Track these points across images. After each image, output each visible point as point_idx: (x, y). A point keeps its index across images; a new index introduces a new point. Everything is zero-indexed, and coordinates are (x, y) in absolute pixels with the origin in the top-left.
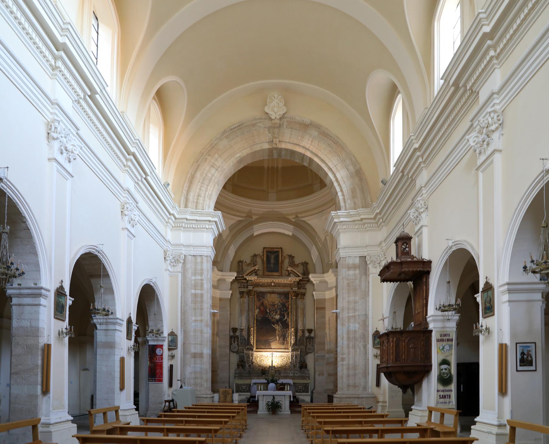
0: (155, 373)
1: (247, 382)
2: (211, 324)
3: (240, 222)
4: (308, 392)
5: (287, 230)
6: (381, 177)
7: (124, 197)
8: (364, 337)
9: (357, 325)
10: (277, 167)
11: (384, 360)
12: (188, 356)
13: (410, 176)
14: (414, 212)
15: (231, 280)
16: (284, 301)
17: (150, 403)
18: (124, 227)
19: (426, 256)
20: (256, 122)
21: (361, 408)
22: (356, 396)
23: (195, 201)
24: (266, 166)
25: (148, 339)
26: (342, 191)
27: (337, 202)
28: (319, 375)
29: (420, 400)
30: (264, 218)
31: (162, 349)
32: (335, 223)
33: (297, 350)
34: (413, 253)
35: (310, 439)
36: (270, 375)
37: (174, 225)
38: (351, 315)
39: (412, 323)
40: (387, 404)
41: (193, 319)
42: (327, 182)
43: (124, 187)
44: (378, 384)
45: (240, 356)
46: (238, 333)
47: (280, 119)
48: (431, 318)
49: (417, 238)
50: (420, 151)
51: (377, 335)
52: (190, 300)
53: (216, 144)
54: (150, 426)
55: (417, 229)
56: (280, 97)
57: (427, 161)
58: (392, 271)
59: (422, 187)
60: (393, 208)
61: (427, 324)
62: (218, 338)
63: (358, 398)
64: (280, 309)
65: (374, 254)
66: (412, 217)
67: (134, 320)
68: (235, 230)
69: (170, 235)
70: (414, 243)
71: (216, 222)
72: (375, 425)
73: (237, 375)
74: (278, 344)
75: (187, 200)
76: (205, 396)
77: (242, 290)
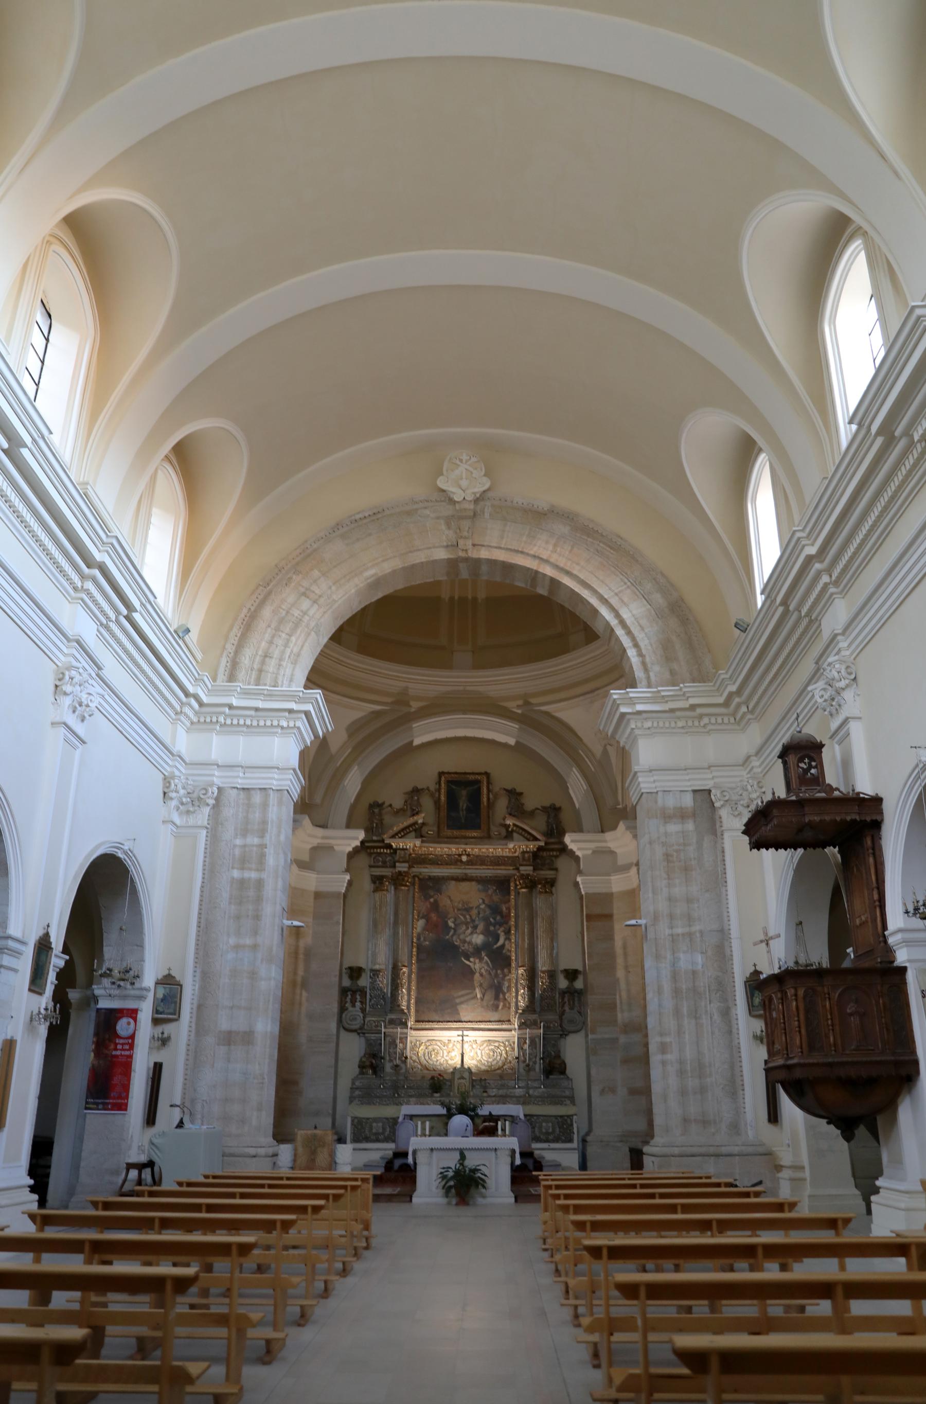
0: (107, 1087)
1: (388, 1111)
2: (281, 955)
3: (376, 714)
4: (570, 1140)
5: (504, 733)
6: (736, 614)
7: (65, 655)
8: (722, 987)
9: (699, 959)
10: (475, 599)
11: (777, 1046)
12: (210, 1040)
13: (804, 611)
14: (824, 689)
15: (350, 849)
16: (496, 898)
17: (82, 1171)
18: (58, 719)
19: (865, 786)
20: (415, 506)
21: (718, 1185)
22: (712, 1150)
23: (255, 666)
24: (445, 595)
25: (97, 992)
26: (636, 645)
27: (627, 670)
28: (602, 1092)
29: (898, 1161)
30: (436, 707)
31: (135, 1020)
32: (623, 715)
33: (533, 1024)
34: (832, 777)
35: (563, 1279)
36: (455, 1094)
37: (195, 720)
38: (679, 931)
39: (850, 950)
40: (807, 1174)
41: (232, 941)
42: (598, 627)
43: (70, 633)
44: (774, 1116)
45: (367, 1040)
46: (364, 981)
47: (476, 501)
48: (899, 936)
49: (837, 747)
50: (822, 562)
51: (757, 984)
52: (226, 895)
53: (315, 550)
54: (52, 1233)
55: (834, 725)
56: (474, 459)
57: (844, 581)
58: (775, 821)
59: (836, 635)
60: (771, 682)
61: (889, 951)
62: (304, 994)
63: (717, 1155)
64: (486, 919)
65: (733, 785)
66: (820, 700)
67: (57, 941)
68: (363, 735)
69: (183, 741)
70: (830, 757)
71: (307, 714)
72: (758, 1233)
73: (357, 1093)
75: (234, 665)
76: (252, 1151)
77: (378, 872)
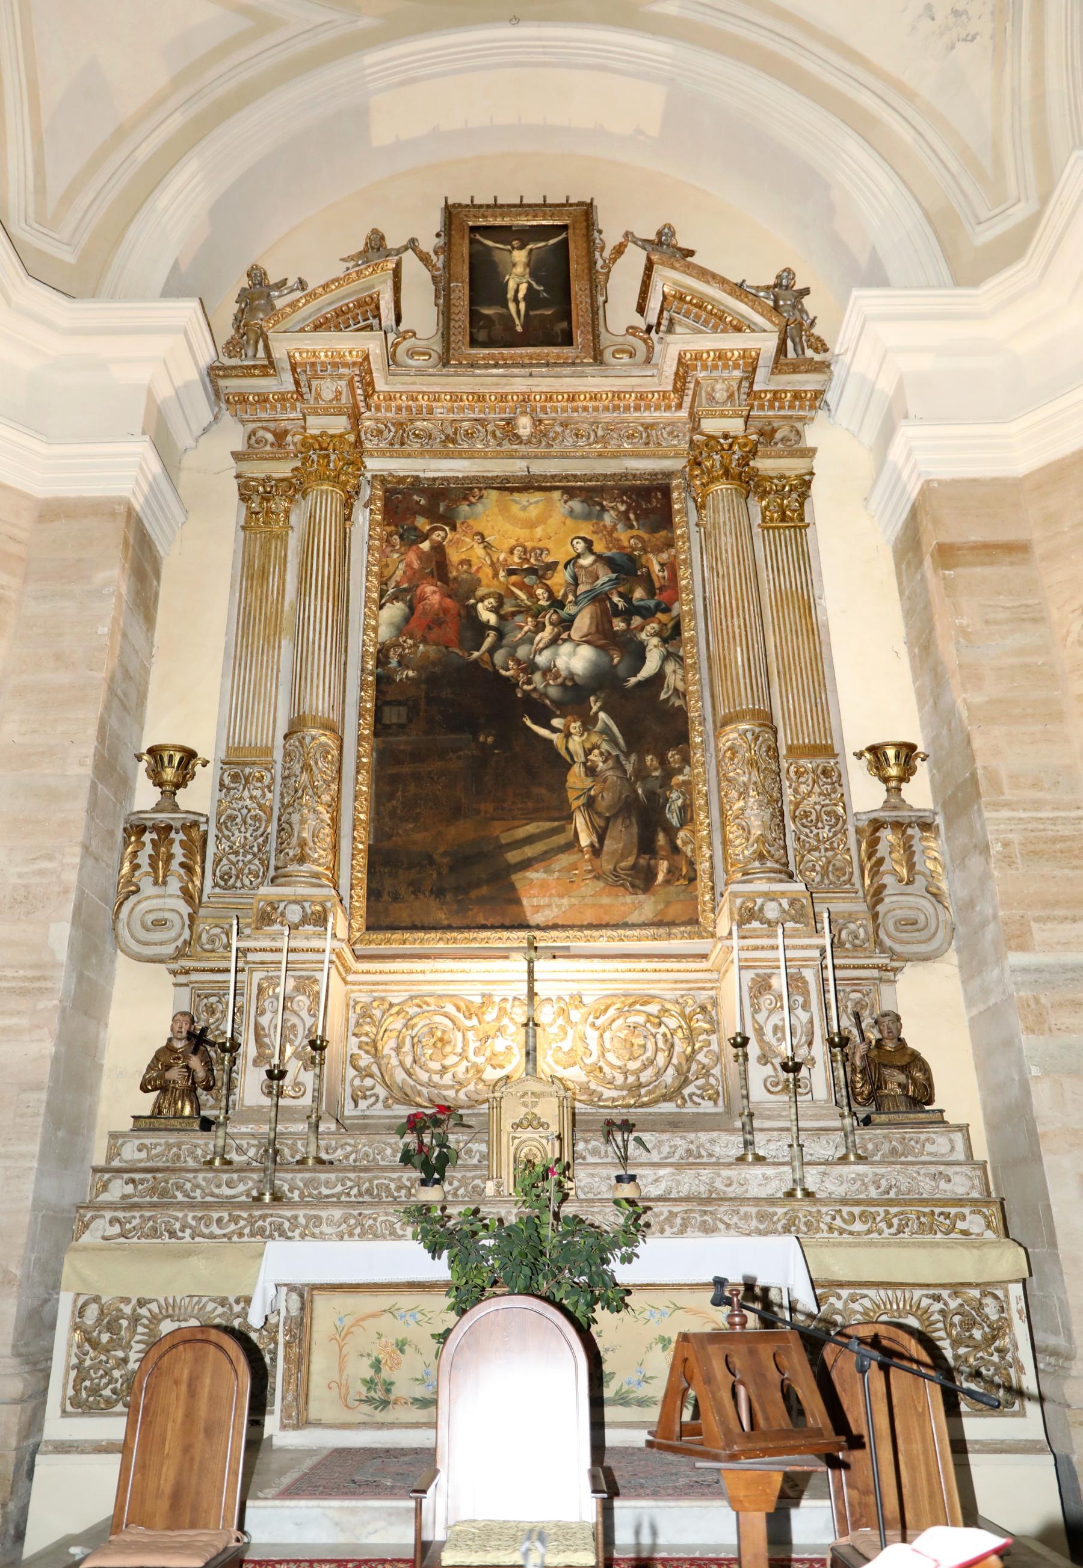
64: (598, 598)
74: (590, 887)
